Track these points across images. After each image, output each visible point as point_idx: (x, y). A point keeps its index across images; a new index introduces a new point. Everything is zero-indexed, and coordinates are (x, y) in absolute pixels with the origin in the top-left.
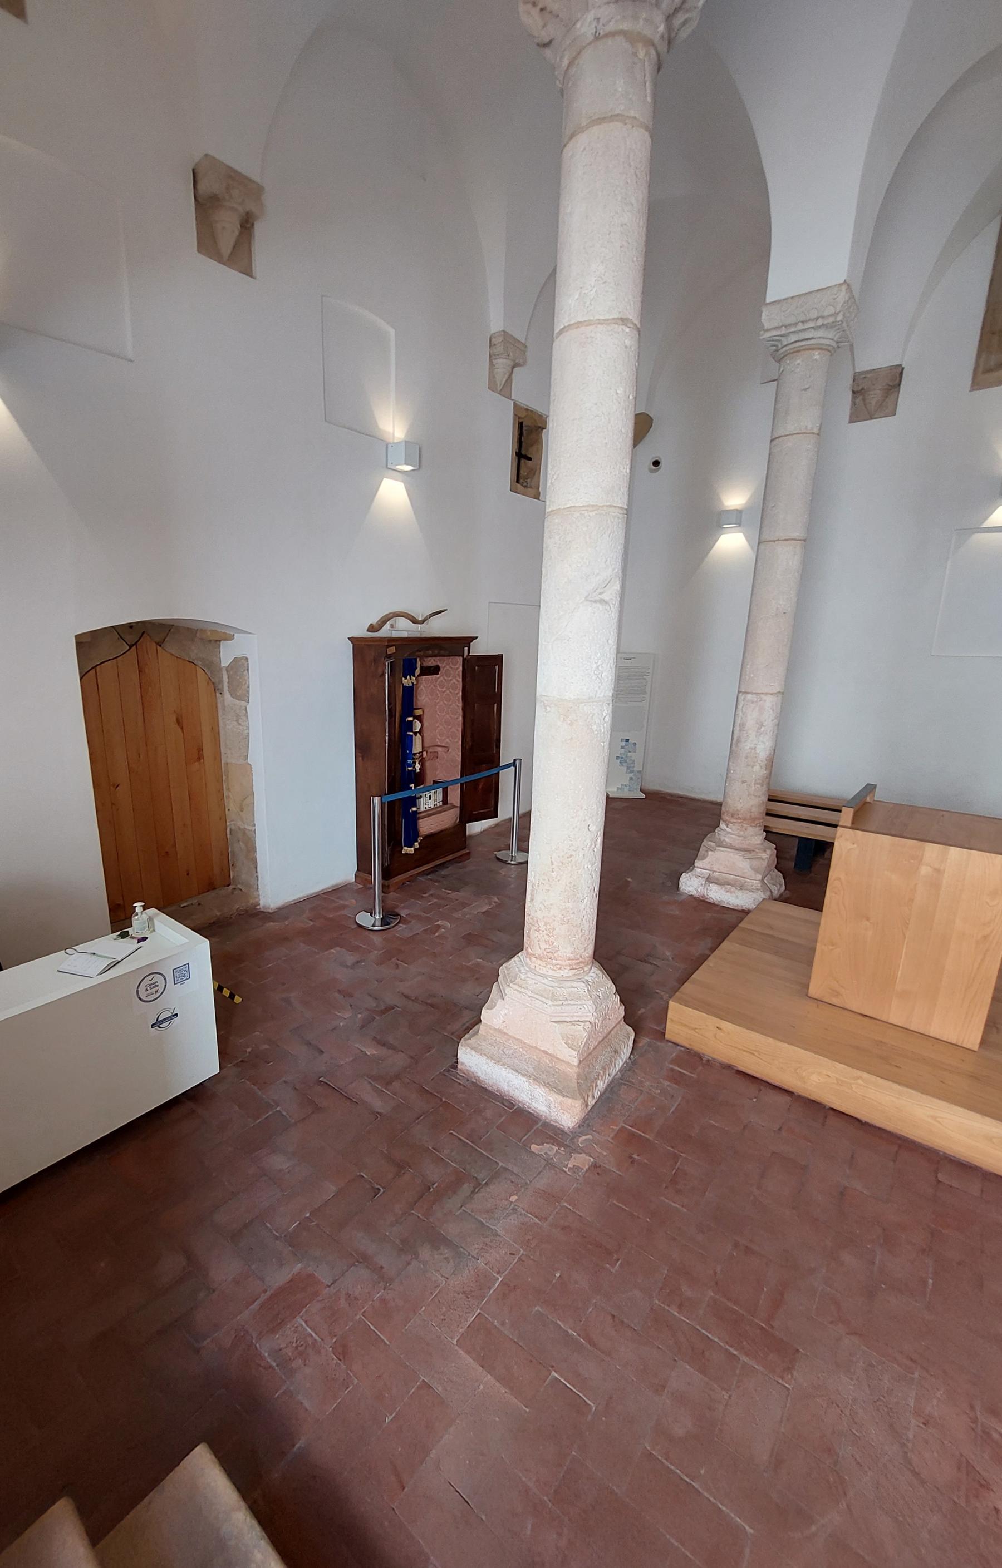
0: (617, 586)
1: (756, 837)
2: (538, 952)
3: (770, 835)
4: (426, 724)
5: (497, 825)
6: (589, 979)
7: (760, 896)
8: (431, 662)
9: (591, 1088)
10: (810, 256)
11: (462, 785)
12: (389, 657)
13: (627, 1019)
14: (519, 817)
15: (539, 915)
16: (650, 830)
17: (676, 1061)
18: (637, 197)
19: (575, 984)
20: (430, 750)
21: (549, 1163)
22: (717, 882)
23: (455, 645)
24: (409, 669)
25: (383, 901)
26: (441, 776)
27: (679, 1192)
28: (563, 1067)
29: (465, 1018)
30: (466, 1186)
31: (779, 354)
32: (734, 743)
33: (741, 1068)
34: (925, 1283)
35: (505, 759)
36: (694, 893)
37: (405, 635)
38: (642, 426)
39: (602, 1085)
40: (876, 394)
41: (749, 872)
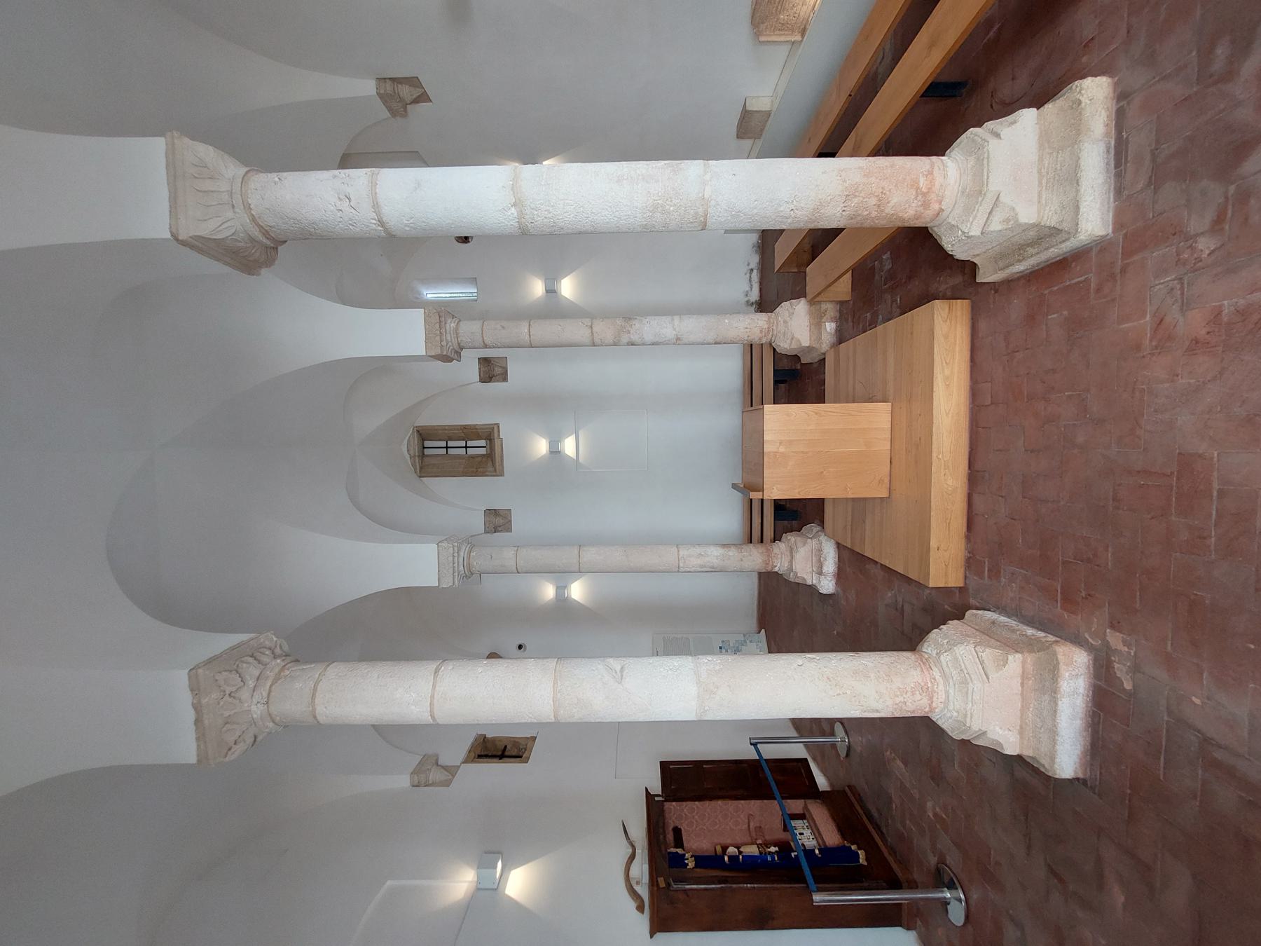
0: (611, 660)
1: (780, 547)
2: (925, 701)
3: (777, 538)
4: (729, 841)
5: (814, 759)
6: (934, 653)
7: (823, 538)
8: (670, 837)
9: (1038, 640)
10: (418, 564)
11: (783, 798)
12: (668, 885)
13: (960, 617)
14: (801, 737)
15: (890, 702)
16: (787, 621)
17: (980, 574)
18: (364, 668)
19: (944, 664)
20: (754, 834)
21: (1136, 669)
22: (821, 566)
23: (654, 809)
24: (678, 861)
25: (926, 887)
26: (778, 823)
27: (1095, 555)
28: (1029, 667)
29: (1023, 775)
30: (1216, 755)
31: (469, 574)
32: (714, 570)
33: (965, 529)
34: (1069, 397)
35: (751, 754)
36: (833, 582)
37: (646, 867)
38: (493, 656)
39: (1030, 631)
40: (498, 521)
41: (807, 548)
